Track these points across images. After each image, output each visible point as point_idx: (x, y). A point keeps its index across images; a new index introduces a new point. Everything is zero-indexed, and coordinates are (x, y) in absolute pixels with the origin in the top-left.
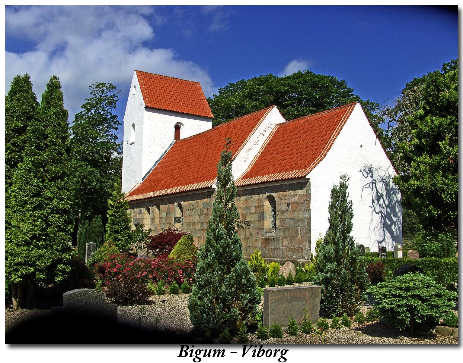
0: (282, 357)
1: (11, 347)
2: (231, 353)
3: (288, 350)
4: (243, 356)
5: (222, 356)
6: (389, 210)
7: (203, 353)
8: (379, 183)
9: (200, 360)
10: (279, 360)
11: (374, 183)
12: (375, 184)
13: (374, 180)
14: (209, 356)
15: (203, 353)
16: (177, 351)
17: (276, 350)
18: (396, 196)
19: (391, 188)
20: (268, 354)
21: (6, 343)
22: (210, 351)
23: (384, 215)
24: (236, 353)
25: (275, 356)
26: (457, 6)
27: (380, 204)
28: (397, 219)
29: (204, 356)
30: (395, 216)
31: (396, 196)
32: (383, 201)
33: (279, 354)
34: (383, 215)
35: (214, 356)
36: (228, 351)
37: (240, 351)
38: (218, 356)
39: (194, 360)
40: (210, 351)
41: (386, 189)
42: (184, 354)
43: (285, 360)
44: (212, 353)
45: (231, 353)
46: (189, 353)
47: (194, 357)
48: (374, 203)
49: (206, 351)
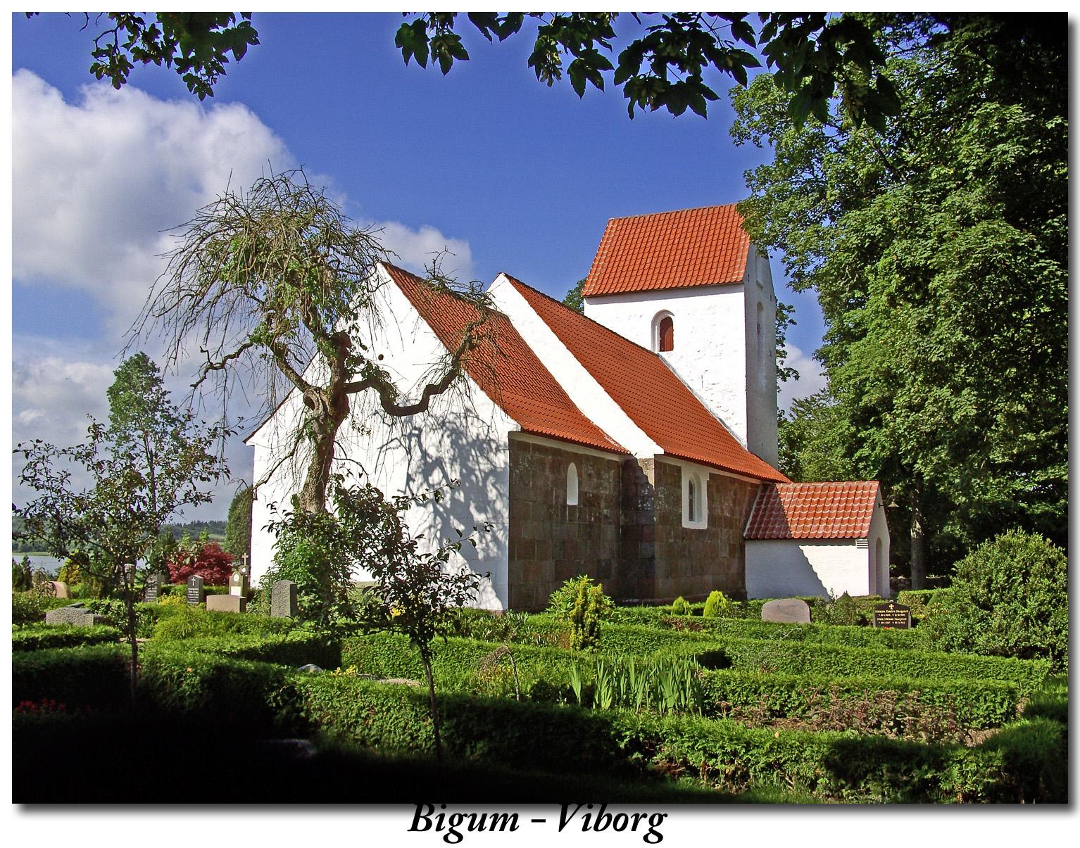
0: (651, 831)
1: (26, 810)
2: (533, 821)
3: (666, 815)
4: (560, 830)
5: (512, 829)
6: (461, 496)
7: (467, 821)
8: (431, 434)
9: (460, 837)
10: (646, 838)
11: (414, 435)
12: (419, 436)
13: (415, 428)
14: (481, 829)
15: (467, 821)
16: (408, 819)
17: (637, 815)
18: (488, 459)
19: (470, 440)
20: (619, 825)
21: (14, 802)
22: (484, 817)
23: (444, 507)
24: (544, 821)
25: (634, 829)
26: (1066, 14)
27: (431, 482)
28: (490, 515)
29: (471, 828)
30: (481, 509)
31: (488, 459)
32: (441, 475)
33: (644, 825)
34: (441, 509)
35: (492, 829)
36: (524, 820)
37: (553, 819)
38: (502, 829)
39: (446, 838)
40: (484, 817)
41: (454, 444)
42: (422, 823)
43: (660, 837)
44: (488, 822)
45: (533, 821)
46: (435, 822)
47: (446, 831)
48: (411, 483)
49: (474, 816)
